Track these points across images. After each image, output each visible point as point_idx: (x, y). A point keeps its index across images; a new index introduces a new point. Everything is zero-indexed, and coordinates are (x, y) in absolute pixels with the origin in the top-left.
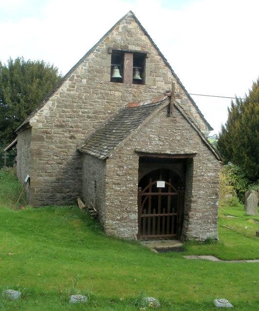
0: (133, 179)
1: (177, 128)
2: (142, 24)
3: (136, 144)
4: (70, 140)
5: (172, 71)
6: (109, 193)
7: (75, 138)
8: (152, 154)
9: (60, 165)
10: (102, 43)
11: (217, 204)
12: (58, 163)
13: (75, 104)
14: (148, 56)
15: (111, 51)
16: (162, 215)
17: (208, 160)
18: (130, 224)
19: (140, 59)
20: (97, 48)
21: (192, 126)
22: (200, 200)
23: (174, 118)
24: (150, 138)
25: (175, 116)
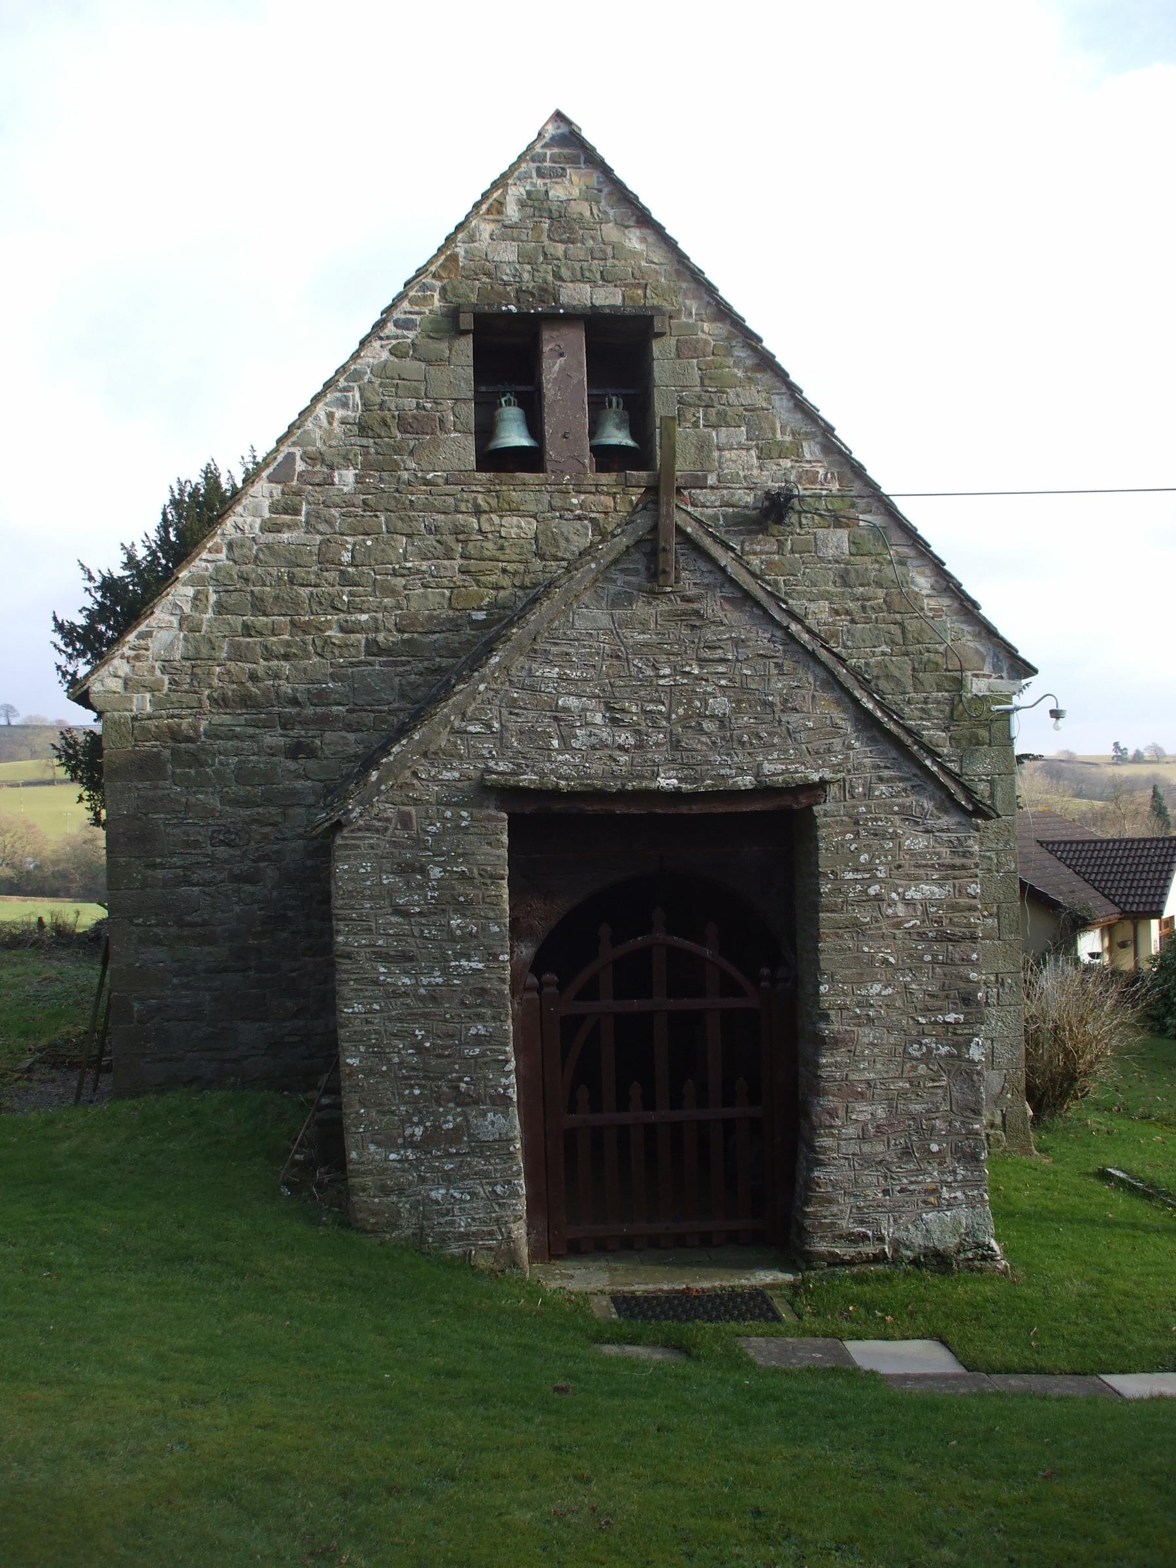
0: (484, 928)
1: (707, 654)
2: (619, 173)
3: (486, 747)
4: (291, 765)
5: (793, 391)
6: (358, 1008)
7: (312, 753)
8: (572, 795)
9: (249, 888)
10: (424, 287)
11: (975, 1053)
12: (236, 878)
13: (304, 592)
14: (658, 326)
15: (467, 321)
16: (652, 1117)
17: (906, 815)
18: (480, 1164)
19: (621, 349)
20: (397, 315)
21: (791, 638)
22: (867, 1035)
23: (688, 600)
24: (558, 715)
25: (691, 592)
